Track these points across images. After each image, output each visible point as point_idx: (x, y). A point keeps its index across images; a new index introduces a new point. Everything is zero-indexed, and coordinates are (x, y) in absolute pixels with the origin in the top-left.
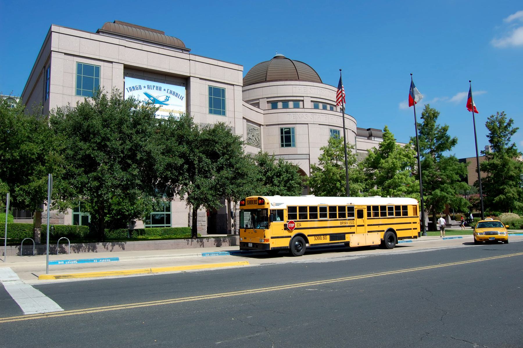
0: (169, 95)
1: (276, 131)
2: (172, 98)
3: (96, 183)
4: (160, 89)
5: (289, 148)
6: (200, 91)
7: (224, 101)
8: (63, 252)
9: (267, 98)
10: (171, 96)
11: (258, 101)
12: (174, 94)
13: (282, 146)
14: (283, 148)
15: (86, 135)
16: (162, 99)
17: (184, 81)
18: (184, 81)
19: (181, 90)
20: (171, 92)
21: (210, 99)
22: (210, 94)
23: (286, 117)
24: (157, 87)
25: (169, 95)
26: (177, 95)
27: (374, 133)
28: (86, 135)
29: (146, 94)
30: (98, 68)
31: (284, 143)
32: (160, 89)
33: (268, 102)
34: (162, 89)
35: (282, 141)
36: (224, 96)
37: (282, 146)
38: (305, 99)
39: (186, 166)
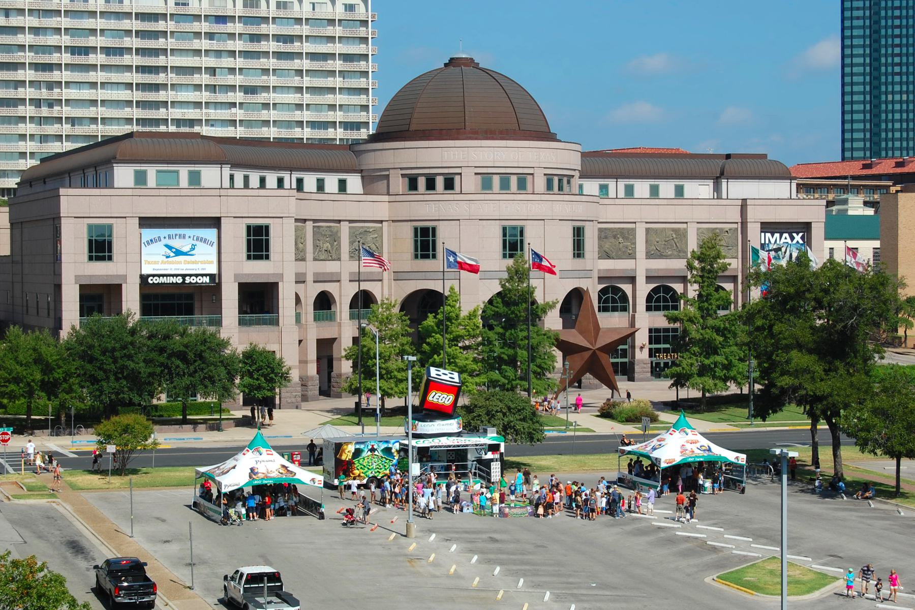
0: (195, 242)
1: (407, 235)
2: (200, 246)
3: (98, 393)
4: (184, 237)
6: (235, 237)
7: (267, 241)
9: (401, 169)
10: (198, 243)
11: (387, 173)
12: (201, 240)
18: (215, 222)
19: (210, 234)
20: (197, 239)
21: (249, 241)
22: (249, 234)
23: (427, 207)
24: (180, 235)
25: (195, 242)
26: (205, 241)
27: (730, 165)
29: (167, 246)
30: (110, 227)
31: (419, 253)
33: (403, 176)
34: (187, 237)
35: (416, 250)
36: (267, 234)
38: (464, 171)
39: (166, 371)
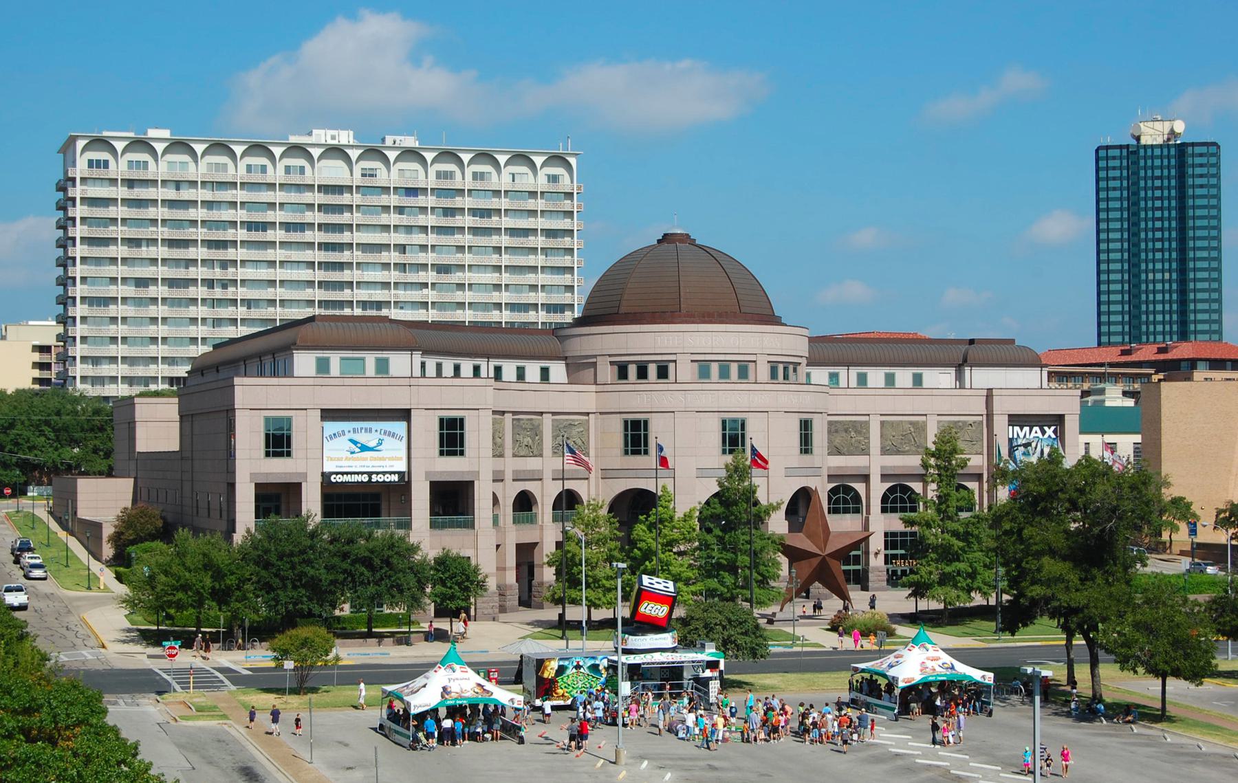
4: (371, 431)
5: (638, 458)
6: (427, 430)
7: (462, 435)
8: (253, 647)
10: (386, 438)
13: (626, 453)
14: (627, 457)
15: (267, 565)
16: (372, 444)
17: (404, 415)
18: (404, 415)
19: (400, 427)
22: (441, 428)
23: (639, 398)
28: (267, 565)
30: (289, 420)
32: (371, 431)
35: (626, 445)
37: (626, 453)
38: (679, 358)
